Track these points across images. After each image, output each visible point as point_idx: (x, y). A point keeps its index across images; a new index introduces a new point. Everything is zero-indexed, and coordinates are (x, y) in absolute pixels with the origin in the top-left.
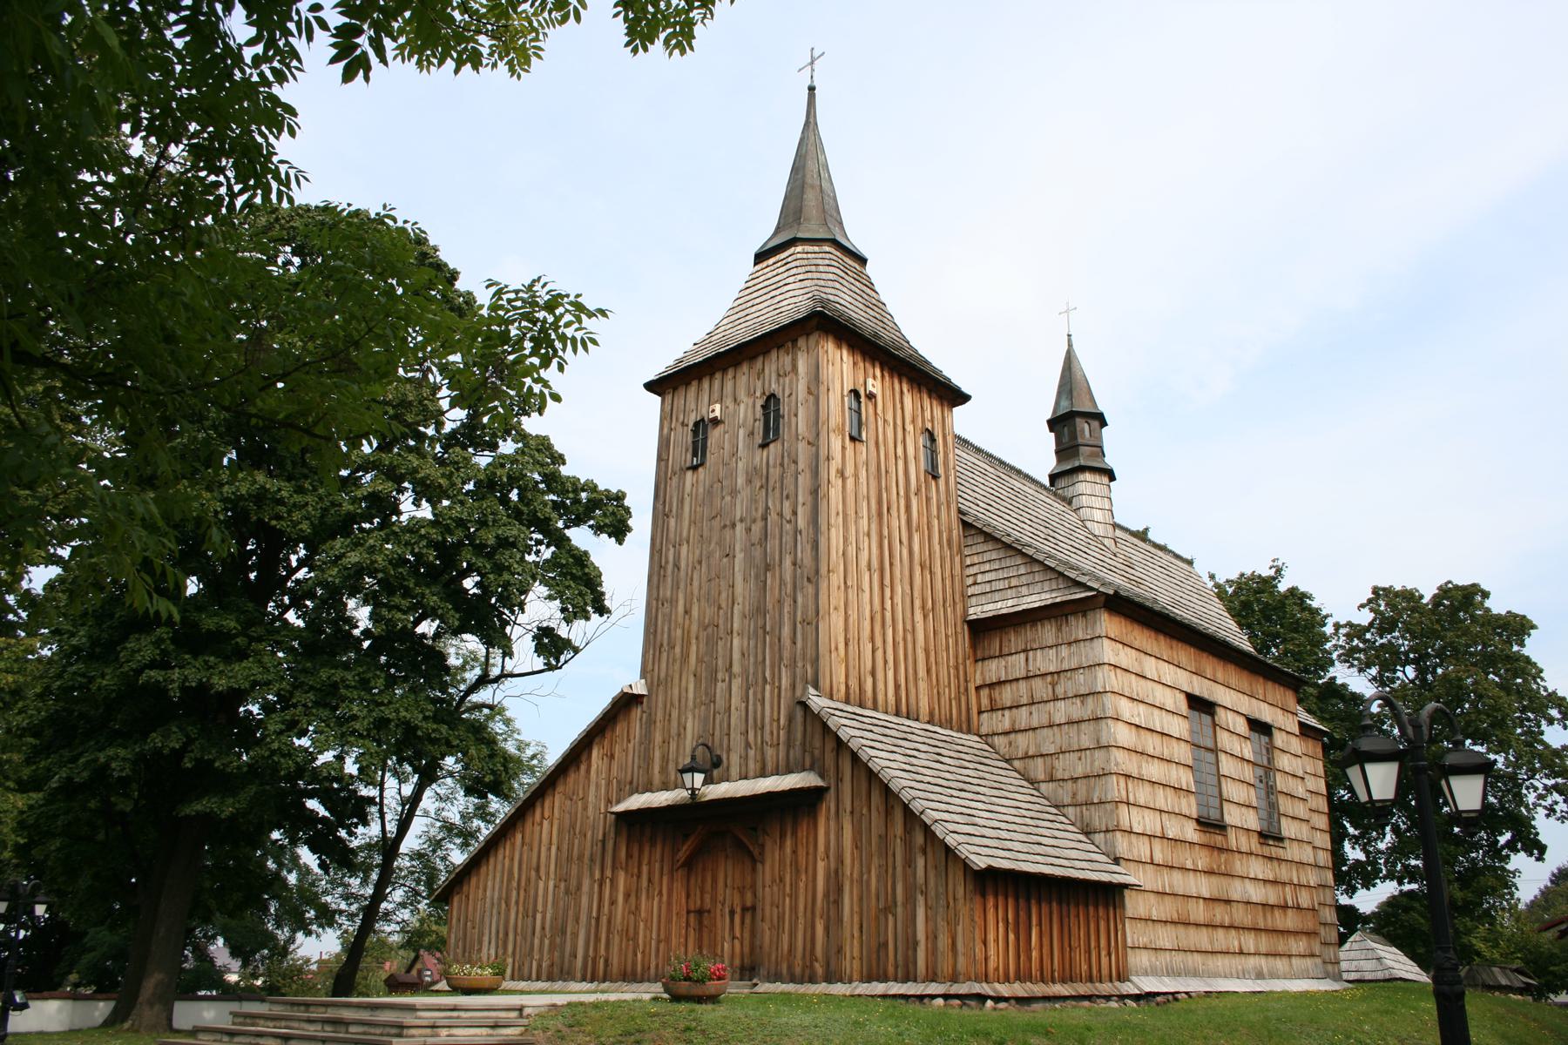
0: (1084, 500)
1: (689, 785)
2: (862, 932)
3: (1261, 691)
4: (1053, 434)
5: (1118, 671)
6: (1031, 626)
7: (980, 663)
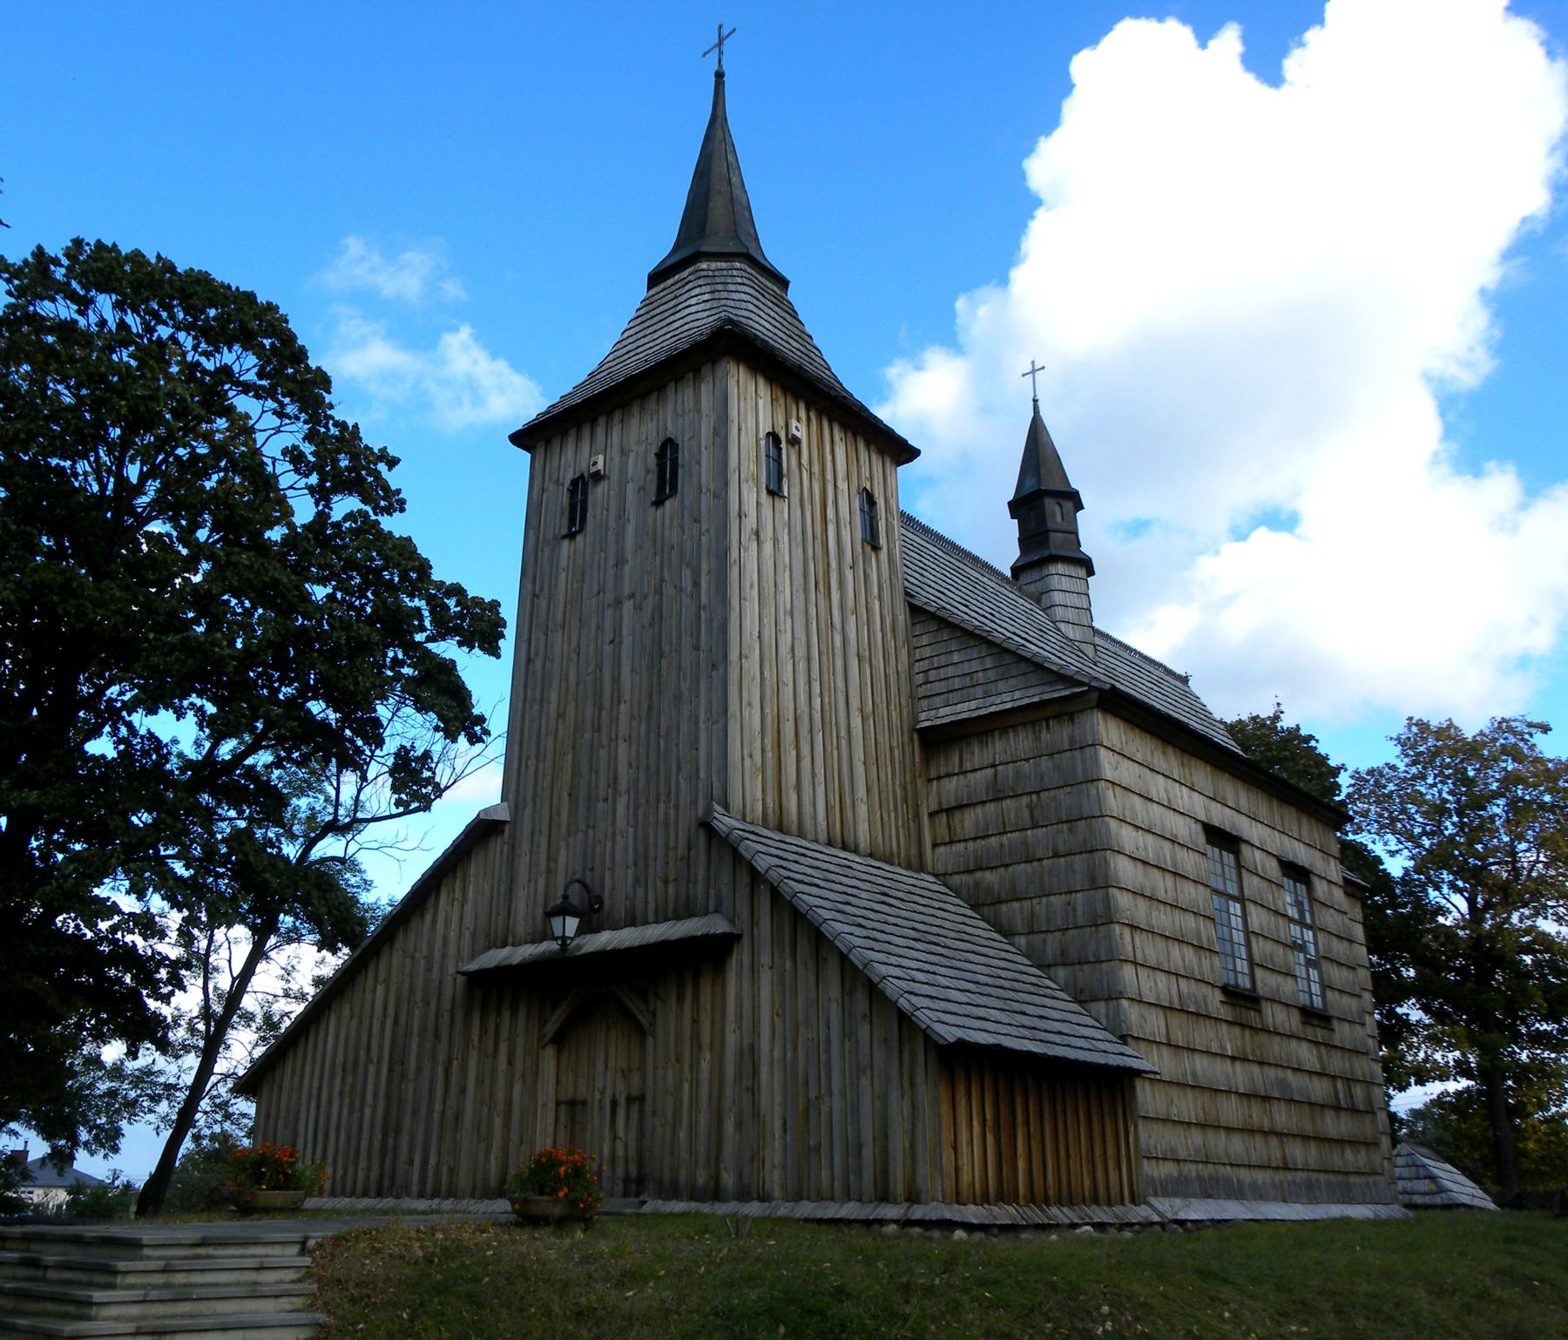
0: (1058, 597)
1: (558, 932)
2: (785, 1131)
3: (1295, 828)
4: (1016, 521)
5: (1117, 789)
6: (1001, 735)
7: (935, 783)
